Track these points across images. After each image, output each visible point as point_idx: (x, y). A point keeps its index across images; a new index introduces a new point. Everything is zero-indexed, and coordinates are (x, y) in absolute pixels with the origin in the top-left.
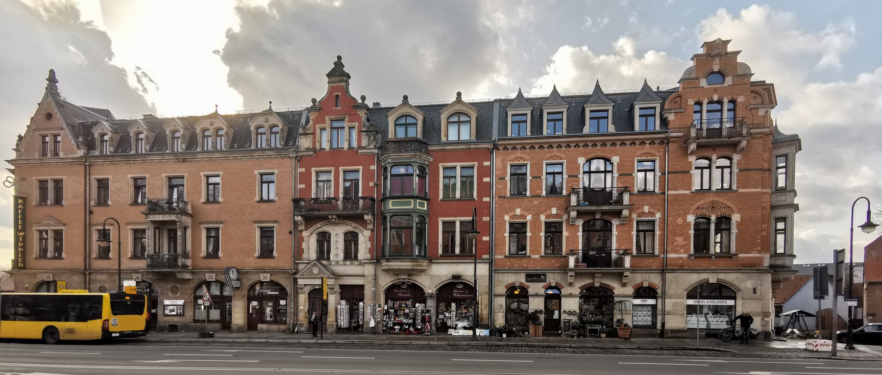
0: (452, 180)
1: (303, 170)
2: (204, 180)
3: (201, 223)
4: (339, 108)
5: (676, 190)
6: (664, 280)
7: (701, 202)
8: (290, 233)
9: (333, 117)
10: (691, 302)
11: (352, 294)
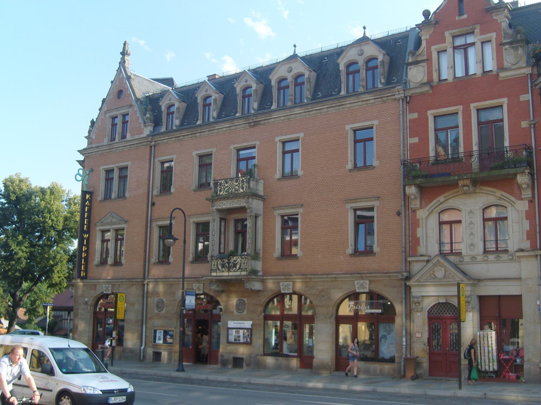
0: (451, 136)
1: (415, 116)
2: (279, 146)
3: (274, 208)
4: (465, 16)
8: (399, 214)
9: (456, 31)
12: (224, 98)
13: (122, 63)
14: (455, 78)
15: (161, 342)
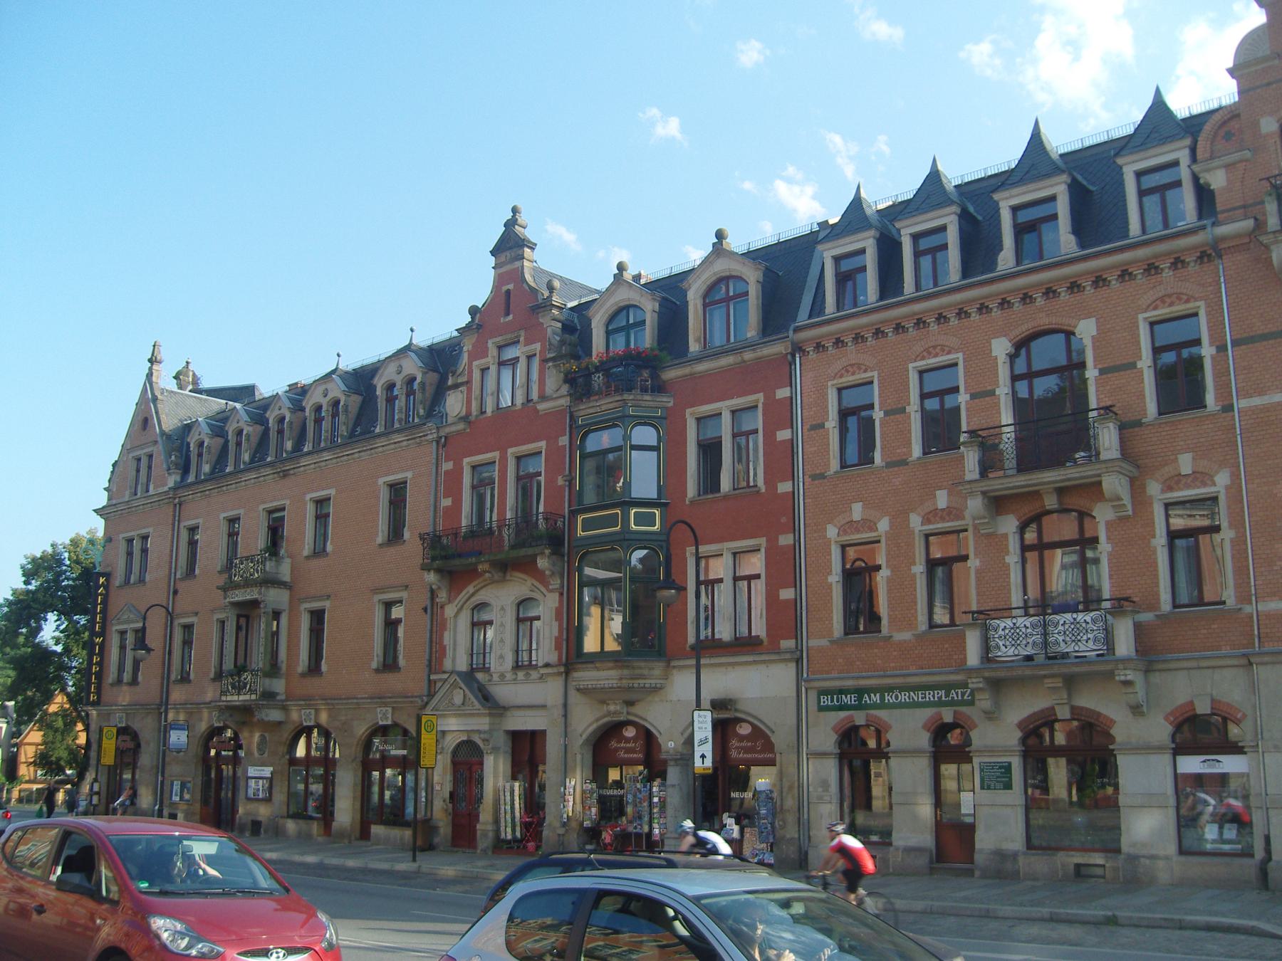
4: (510, 317)
5: (1261, 393)
6: (1253, 687)
8: (425, 610)
10: (1191, 764)
11: (527, 751)
12: (363, 401)
13: (150, 375)
14: (498, 408)
15: (178, 799)
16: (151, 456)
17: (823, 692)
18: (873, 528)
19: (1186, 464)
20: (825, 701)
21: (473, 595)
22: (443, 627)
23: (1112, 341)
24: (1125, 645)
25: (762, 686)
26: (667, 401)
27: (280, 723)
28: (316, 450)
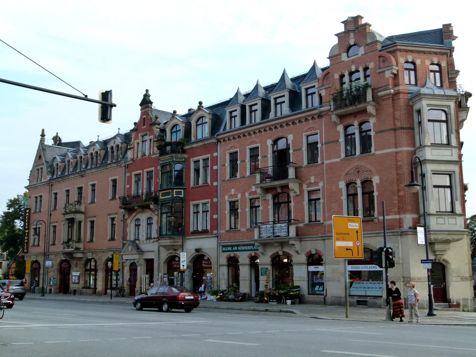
4: (145, 127)
7: (349, 168)
9: (142, 134)
10: (312, 268)
16: (42, 169)
17: (223, 246)
18: (237, 197)
19: (312, 179)
20: (224, 249)
21: (135, 216)
22: (127, 226)
23: (295, 141)
24: (293, 232)
25: (209, 245)
26: (186, 156)
27: (82, 258)
28: (92, 168)
